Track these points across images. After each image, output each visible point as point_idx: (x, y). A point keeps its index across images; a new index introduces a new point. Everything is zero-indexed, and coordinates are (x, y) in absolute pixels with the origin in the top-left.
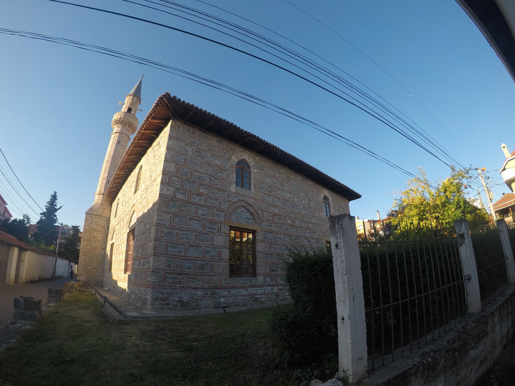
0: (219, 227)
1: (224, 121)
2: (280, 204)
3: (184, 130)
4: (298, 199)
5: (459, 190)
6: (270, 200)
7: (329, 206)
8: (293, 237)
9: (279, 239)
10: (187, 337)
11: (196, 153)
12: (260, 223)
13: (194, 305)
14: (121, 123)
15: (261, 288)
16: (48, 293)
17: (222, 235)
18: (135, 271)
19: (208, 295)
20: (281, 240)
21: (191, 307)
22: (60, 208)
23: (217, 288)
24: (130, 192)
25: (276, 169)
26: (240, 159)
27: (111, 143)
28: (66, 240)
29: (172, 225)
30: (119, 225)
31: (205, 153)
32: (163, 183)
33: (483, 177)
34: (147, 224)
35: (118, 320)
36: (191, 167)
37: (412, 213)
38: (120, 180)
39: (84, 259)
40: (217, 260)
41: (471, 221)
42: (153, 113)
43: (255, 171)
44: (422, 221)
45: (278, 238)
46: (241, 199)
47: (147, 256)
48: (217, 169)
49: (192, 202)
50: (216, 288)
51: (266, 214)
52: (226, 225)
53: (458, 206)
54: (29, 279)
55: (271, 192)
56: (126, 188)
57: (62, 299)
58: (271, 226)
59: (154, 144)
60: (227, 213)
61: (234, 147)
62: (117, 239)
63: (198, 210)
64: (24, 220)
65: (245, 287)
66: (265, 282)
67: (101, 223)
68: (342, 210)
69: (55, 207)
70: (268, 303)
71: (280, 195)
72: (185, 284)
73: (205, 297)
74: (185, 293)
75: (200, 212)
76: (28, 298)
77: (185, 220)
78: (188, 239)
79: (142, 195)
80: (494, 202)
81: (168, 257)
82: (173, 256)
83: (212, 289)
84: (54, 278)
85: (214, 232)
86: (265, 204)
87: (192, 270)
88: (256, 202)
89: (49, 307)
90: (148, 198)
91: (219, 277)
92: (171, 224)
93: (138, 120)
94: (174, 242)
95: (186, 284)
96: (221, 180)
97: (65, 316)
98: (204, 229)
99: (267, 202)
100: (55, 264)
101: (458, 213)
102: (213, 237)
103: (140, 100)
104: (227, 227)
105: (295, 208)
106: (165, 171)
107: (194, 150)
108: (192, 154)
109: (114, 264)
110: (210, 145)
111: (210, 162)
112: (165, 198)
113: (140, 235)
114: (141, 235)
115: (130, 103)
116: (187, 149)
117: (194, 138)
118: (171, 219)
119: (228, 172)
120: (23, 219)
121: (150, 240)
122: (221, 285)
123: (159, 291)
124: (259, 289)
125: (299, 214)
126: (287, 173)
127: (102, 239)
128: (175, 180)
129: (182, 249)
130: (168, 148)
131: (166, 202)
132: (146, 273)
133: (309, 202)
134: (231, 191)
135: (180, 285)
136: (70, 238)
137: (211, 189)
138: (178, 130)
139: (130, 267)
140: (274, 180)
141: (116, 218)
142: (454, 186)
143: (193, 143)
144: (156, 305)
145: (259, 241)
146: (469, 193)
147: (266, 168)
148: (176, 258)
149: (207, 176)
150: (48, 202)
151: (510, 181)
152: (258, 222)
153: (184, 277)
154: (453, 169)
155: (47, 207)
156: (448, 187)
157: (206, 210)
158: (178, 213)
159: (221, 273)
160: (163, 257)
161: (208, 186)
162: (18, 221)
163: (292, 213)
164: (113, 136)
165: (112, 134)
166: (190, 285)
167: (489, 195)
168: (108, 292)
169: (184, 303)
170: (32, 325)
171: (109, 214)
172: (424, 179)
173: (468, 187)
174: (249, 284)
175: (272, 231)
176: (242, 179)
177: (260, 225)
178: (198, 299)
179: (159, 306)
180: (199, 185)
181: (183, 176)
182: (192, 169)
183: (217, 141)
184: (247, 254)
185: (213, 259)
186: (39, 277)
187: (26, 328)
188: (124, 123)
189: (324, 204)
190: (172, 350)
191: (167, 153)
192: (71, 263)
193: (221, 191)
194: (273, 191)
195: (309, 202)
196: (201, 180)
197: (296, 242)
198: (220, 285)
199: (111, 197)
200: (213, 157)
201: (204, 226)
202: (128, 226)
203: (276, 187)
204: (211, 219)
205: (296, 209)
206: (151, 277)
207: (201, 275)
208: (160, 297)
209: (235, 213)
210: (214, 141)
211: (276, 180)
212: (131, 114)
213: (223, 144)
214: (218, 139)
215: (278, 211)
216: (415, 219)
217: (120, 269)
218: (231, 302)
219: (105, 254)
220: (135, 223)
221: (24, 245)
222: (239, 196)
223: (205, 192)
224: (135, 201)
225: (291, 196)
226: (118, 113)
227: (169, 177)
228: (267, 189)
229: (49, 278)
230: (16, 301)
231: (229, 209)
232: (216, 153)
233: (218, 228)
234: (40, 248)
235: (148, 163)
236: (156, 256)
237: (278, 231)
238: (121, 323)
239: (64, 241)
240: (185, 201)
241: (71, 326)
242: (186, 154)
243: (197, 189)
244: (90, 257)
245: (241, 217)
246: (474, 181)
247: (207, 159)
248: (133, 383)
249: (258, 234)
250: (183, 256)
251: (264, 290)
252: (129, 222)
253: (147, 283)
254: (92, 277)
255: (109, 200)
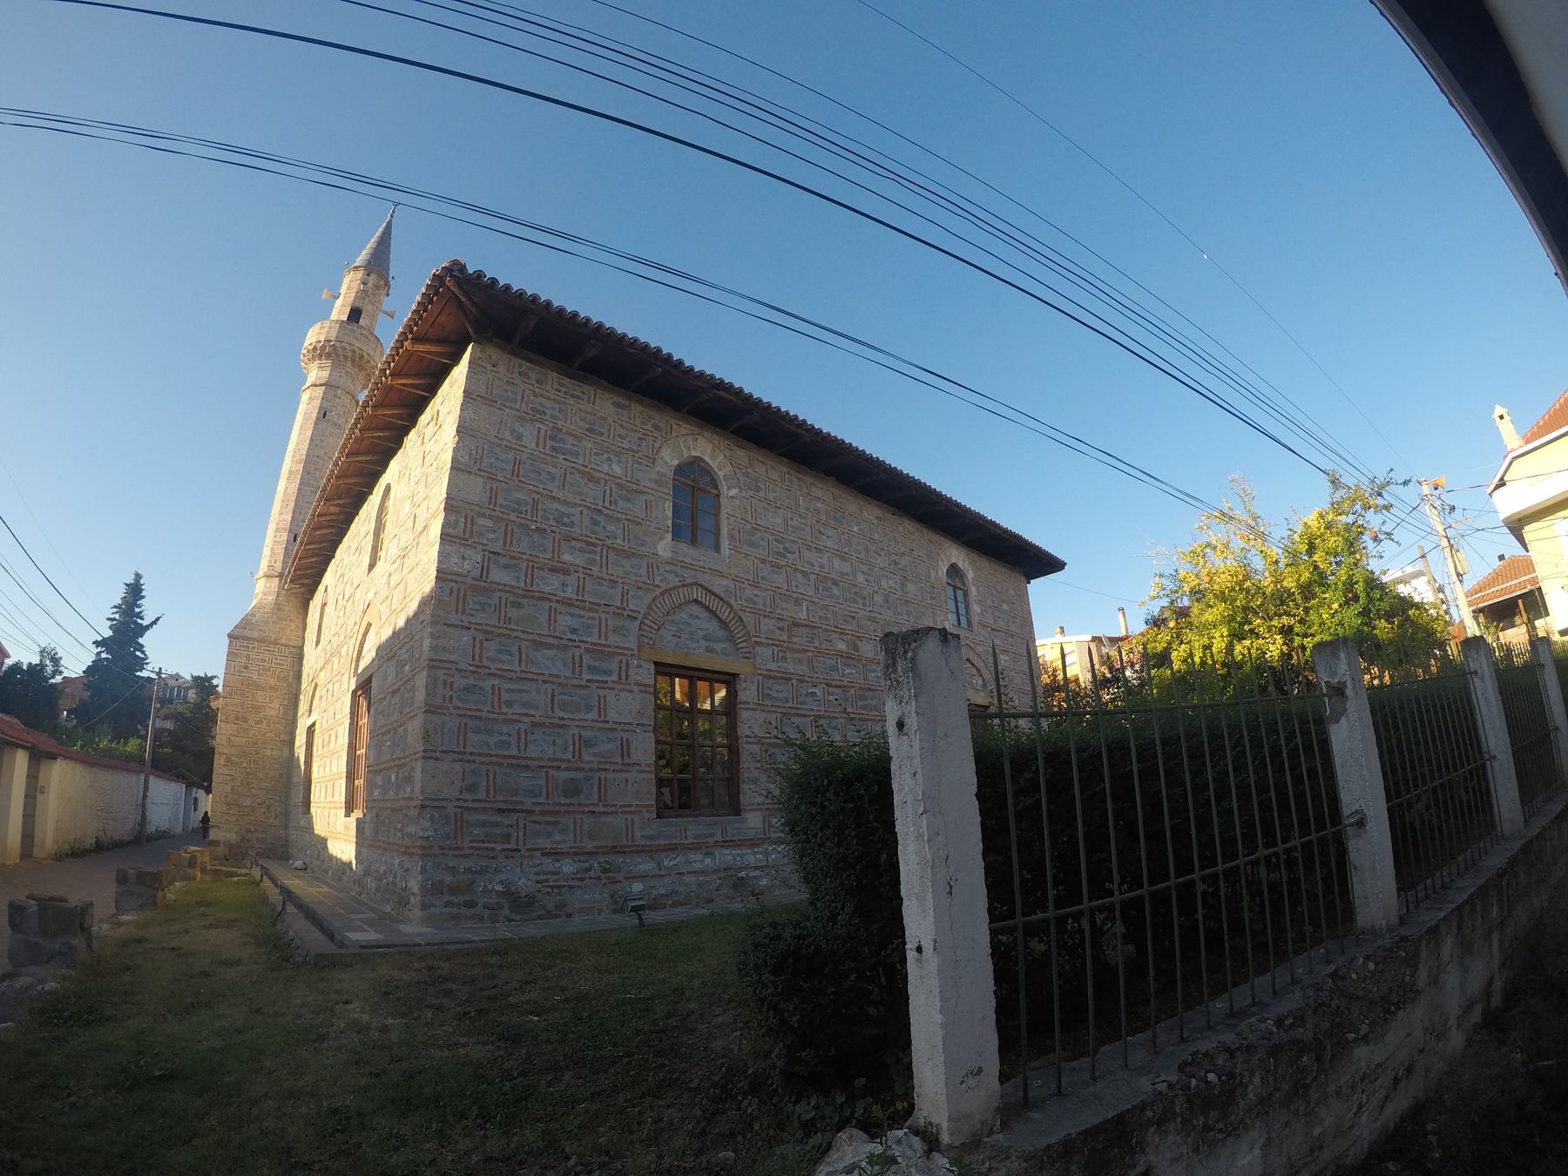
0: (623, 666)
1: (634, 342)
2: (811, 591)
3: (512, 373)
4: (868, 578)
5: (1352, 545)
6: (779, 580)
7: (966, 595)
8: (852, 691)
9: (810, 699)
10: (512, 1000)
11: (549, 443)
12: (750, 652)
13: (550, 906)
14: (328, 356)
15: (756, 850)
16: (116, 885)
17: (631, 691)
18: (375, 807)
19: (592, 874)
20: (815, 701)
21: (543, 912)
22: (154, 622)
23: (619, 852)
24: (358, 567)
25: (799, 486)
26: (686, 456)
27: (299, 418)
28: (175, 724)
29: (477, 662)
30: (329, 667)
31: (576, 443)
32: (449, 538)
33: (1435, 508)
34: (403, 663)
35: (316, 955)
36: (533, 485)
37: (1209, 616)
38: (329, 531)
39: (228, 778)
40: (619, 767)
41: (1388, 639)
42: (416, 325)
43: (733, 492)
44: (1241, 639)
45: (807, 695)
46: (689, 581)
47: (407, 760)
48: (613, 489)
49: (538, 591)
50: (617, 851)
51: (768, 624)
52: (644, 660)
53: (1350, 595)
54: (67, 846)
55: (785, 556)
56: (347, 554)
57: (158, 901)
58: (784, 659)
59: (424, 419)
60: (646, 621)
61: (667, 421)
62: (325, 711)
63: (555, 616)
64: (42, 666)
65: (707, 847)
66: (767, 830)
67: (275, 664)
68: (1005, 607)
69: (139, 621)
70: (777, 892)
71: (812, 565)
72: (521, 842)
73: (582, 880)
74: (521, 868)
75: (565, 621)
76: (52, 899)
77: (517, 647)
78: (527, 705)
79: (390, 575)
80: (1471, 582)
81: (469, 761)
82: (483, 759)
83: (604, 853)
84: (142, 839)
85: (607, 682)
86: (763, 594)
87: (542, 800)
88: (738, 587)
89: (119, 924)
90: (406, 583)
91: (626, 819)
92: (474, 660)
93: (381, 344)
94: (484, 715)
95: (525, 840)
96: (626, 522)
97: (163, 948)
98: (578, 673)
99: (770, 587)
100: (145, 797)
101: (1351, 617)
102: (605, 697)
103: (387, 284)
104: (647, 667)
105: (858, 603)
106: (453, 499)
107: (542, 434)
108: (537, 446)
109: (318, 787)
110: (591, 417)
111: (594, 469)
112: (456, 582)
113: (385, 698)
114: (388, 698)
115: (357, 293)
116: (521, 430)
117: (542, 396)
118: (474, 647)
119: (649, 498)
120: (41, 661)
121: (412, 711)
122: (633, 841)
123: (444, 866)
124: (750, 851)
125: (869, 623)
126: (832, 497)
127: (281, 712)
128: (484, 526)
129: (509, 735)
130: (461, 430)
131: (458, 595)
132: (405, 812)
133: (903, 585)
134: (657, 554)
135: (507, 846)
136: (189, 715)
137: (596, 552)
138: (493, 373)
139: (360, 797)
140: (792, 519)
141: (320, 646)
142: (1338, 534)
143: (538, 412)
144: (434, 906)
145: (747, 706)
146: (1381, 557)
147: (767, 483)
148: (492, 763)
149: (582, 511)
150: (115, 607)
151: (1520, 520)
152: (742, 648)
153: (518, 819)
154: (1335, 483)
155: (115, 622)
156: (1320, 537)
157: (583, 617)
158: (495, 626)
159: (632, 806)
160: (454, 761)
161: (589, 544)
162: (25, 667)
163: (850, 619)
164: (305, 396)
165: (303, 388)
166: (537, 843)
167: (1454, 562)
168: (301, 873)
169: (520, 897)
170: (64, 979)
171: (299, 637)
172: (1250, 511)
173: (1383, 537)
174: (719, 837)
175: (787, 676)
176: (693, 518)
177: (749, 658)
178: (564, 886)
179: (446, 910)
180: (559, 539)
181: (509, 514)
182: (538, 493)
183: (614, 404)
184: (712, 747)
185: (606, 763)
186: (97, 837)
187: (46, 988)
188: (338, 355)
189: (950, 590)
190: (462, 1040)
191: (460, 444)
192: (195, 790)
193: (628, 555)
194: (789, 553)
195: (903, 585)
196: (564, 524)
197: (861, 708)
198: (627, 840)
199: (303, 585)
200: (602, 455)
201: (577, 665)
202: (352, 670)
203: (800, 541)
204: (597, 641)
205: (862, 607)
206: (418, 824)
207: (568, 812)
208: (448, 882)
209: (673, 622)
210: (603, 406)
211: (799, 520)
212: (362, 327)
213: (633, 411)
214: (616, 399)
215: (804, 615)
216: (1217, 635)
217: (335, 802)
218: (664, 892)
219: (291, 759)
220: (373, 660)
221: (44, 741)
222: (684, 570)
223: (578, 561)
224: (370, 595)
225: (847, 568)
226: (319, 324)
227: (466, 519)
228: (771, 546)
229: (128, 838)
230: (15, 910)
231: (652, 609)
232: (611, 441)
233: (620, 668)
234: (94, 750)
235: (406, 478)
236: (431, 761)
237: (804, 676)
238: (326, 963)
239: (169, 725)
240: (516, 590)
241: (178, 977)
242: (519, 445)
243: (553, 553)
244: (248, 770)
245: (692, 634)
246: (1408, 519)
247: (584, 461)
248: (337, 1135)
249: (744, 685)
250: (513, 757)
251: (766, 854)
252: (355, 657)
253: (407, 842)
254: (256, 831)
255: (297, 592)
